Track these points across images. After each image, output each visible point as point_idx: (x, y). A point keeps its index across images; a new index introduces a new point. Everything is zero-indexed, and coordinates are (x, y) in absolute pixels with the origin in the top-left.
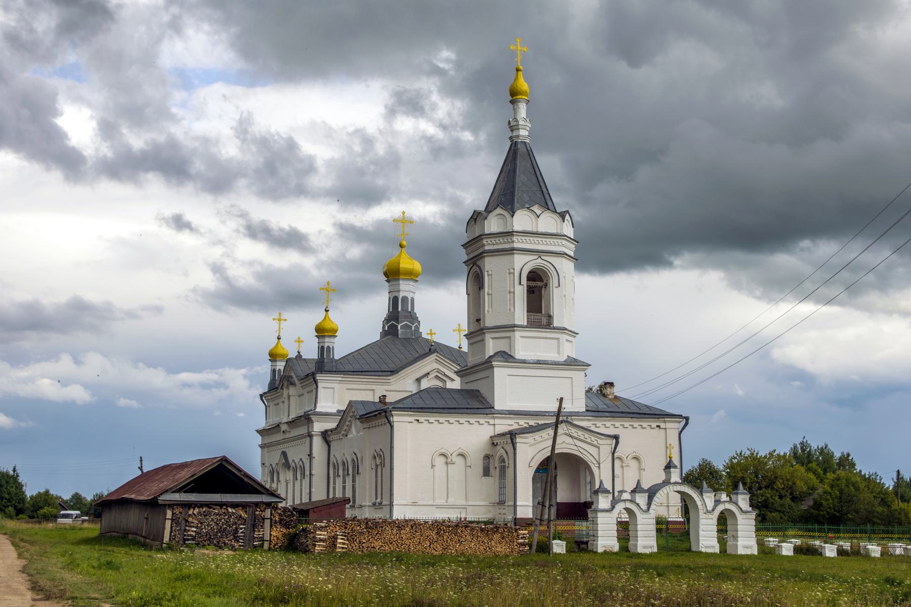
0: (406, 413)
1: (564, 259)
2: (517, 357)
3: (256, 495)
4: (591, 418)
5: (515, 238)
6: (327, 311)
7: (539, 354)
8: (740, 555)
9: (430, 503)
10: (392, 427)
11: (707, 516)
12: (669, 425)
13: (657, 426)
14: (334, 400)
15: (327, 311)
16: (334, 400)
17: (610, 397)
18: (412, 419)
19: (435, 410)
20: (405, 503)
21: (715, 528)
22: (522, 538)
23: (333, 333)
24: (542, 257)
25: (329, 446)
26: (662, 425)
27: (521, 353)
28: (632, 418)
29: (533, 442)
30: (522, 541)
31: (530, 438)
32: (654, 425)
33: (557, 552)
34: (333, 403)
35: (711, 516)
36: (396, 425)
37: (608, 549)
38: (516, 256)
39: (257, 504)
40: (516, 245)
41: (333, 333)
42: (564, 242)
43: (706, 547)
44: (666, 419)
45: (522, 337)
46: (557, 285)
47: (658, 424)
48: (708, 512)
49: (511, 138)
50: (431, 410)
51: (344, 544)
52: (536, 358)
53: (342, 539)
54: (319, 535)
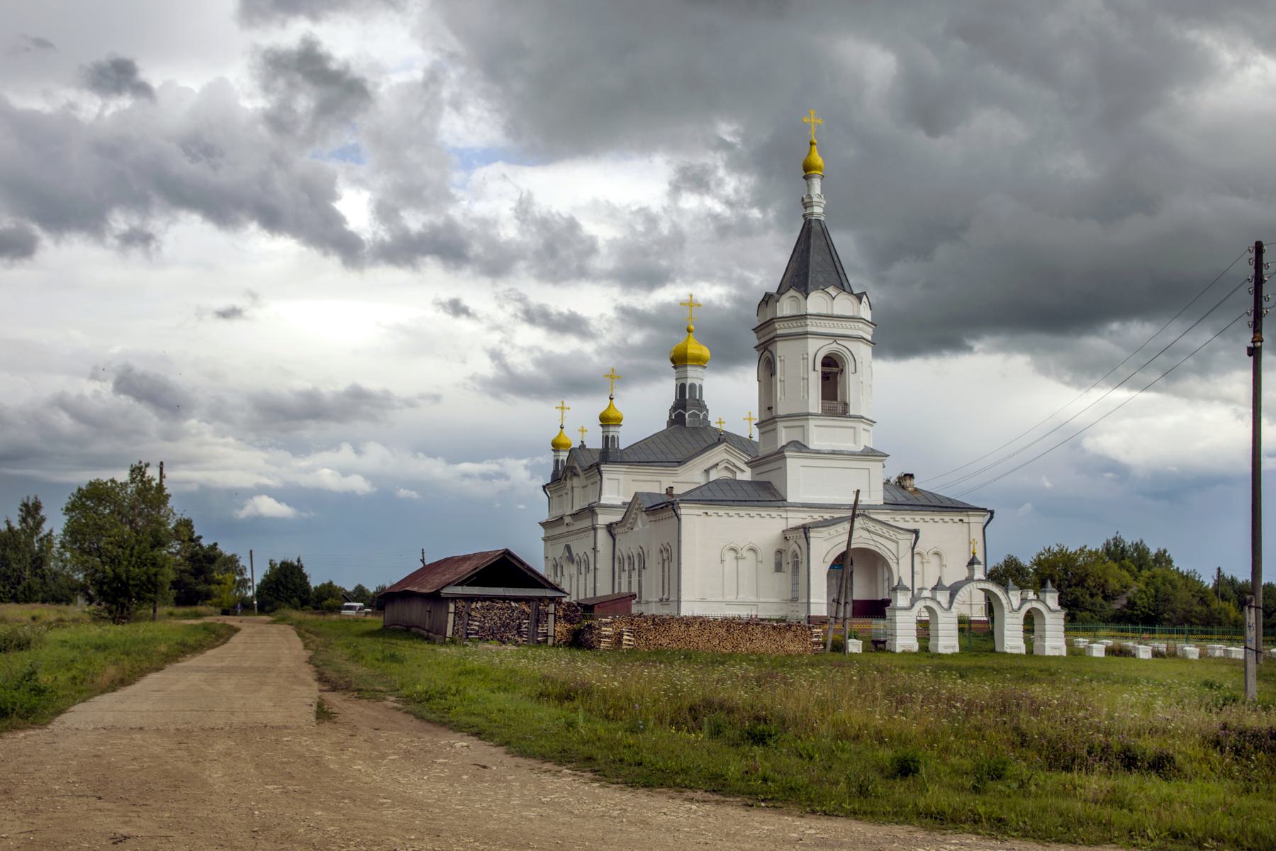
10: (679, 520)
12: (972, 519)
13: (960, 520)
15: (611, 399)
22: (816, 637)
23: (617, 422)
25: (614, 540)
29: (828, 536)
30: (816, 639)
31: (824, 532)
32: (956, 519)
36: (683, 518)
37: (907, 649)
38: (810, 340)
39: (541, 599)
41: (617, 422)
43: (1011, 648)
45: (816, 426)
46: (853, 371)
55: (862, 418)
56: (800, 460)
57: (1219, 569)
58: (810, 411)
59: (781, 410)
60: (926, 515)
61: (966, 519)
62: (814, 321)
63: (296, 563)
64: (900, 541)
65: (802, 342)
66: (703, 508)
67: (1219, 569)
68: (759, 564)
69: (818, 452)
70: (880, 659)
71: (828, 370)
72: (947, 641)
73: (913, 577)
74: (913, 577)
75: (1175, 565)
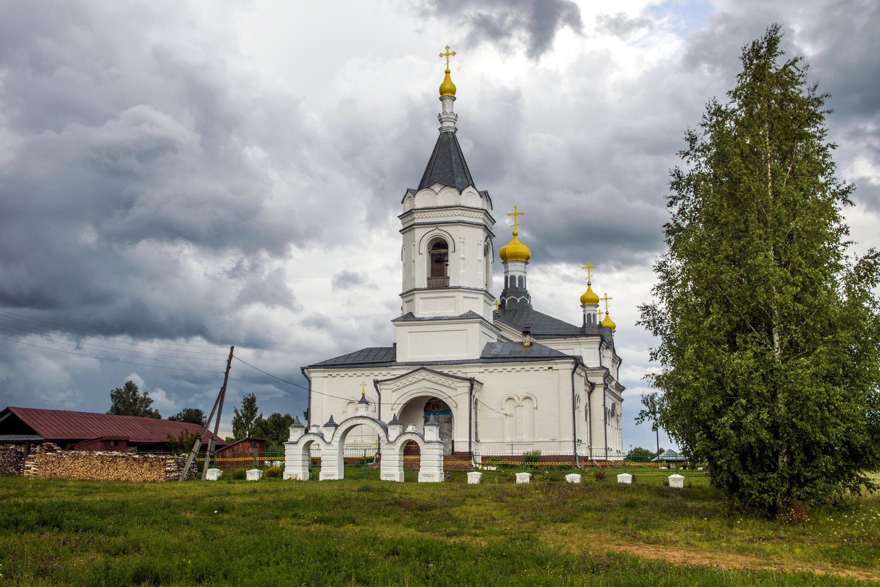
0: (319, 369)
1: (460, 227)
2: (416, 316)
3: (24, 435)
4: (480, 364)
5: (415, 215)
6: (589, 285)
7: (436, 312)
8: (621, 483)
9: (501, 440)
10: (310, 381)
11: (389, 446)
12: (560, 366)
13: (549, 368)
14: (483, 358)
15: (589, 285)
16: (483, 358)
17: (526, 344)
18: (326, 374)
19: (344, 366)
20: (548, 440)
21: (422, 458)
22: (168, 466)
23: (595, 302)
24: (439, 228)
25: (379, 395)
26: (554, 367)
27: (420, 313)
28: (522, 362)
29: (395, 388)
30: (169, 468)
31: (392, 386)
32: (546, 367)
33: (210, 479)
34: (595, 360)
35: (392, 447)
36: (313, 380)
37: (293, 477)
38: (416, 230)
39: (30, 442)
40: (416, 221)
41: (595, 302)
42: (460, 212)
43: (386, 475)
44: (556, 361)
45: (422, 298)
46: (453, 250)
47: (550, 366)
48: (390, 443)
49: (440, 129)
50: (341, 366)
51: (35, 471)
52: (432, 316)
53: (35, 467)
54: (27, 464)
55: (459, 287)
56: (408, 327)
57: (332, 416)
58: (416, 287)
59: (482, 286)
60: (334, 371)
61: (554, 367)
62: (419, 214)
63: (203, 416)
64: (458, 389)
65: (412, 231)
66: (328, 371)
67: (332, 416)
68: (390, 406)
69: (420, 320)
70: (274, 485)
71: (437, 252)
72: (332, 471)
73: (574, 413)
74: (574, 413)
75: (163, 418)
